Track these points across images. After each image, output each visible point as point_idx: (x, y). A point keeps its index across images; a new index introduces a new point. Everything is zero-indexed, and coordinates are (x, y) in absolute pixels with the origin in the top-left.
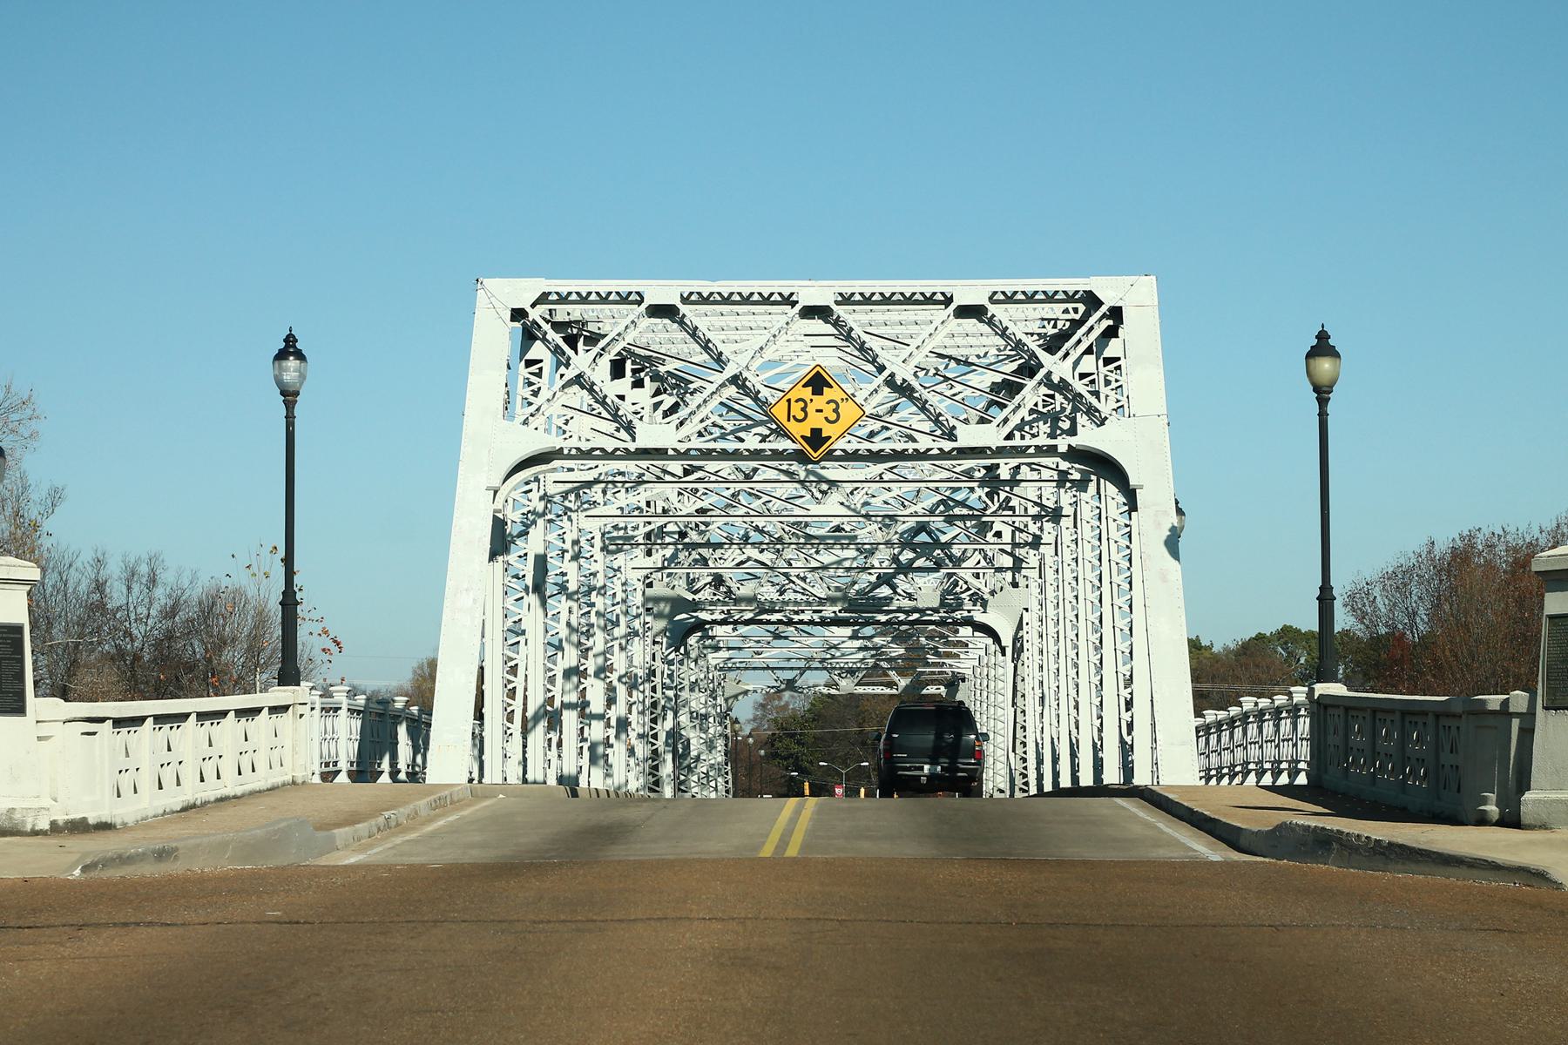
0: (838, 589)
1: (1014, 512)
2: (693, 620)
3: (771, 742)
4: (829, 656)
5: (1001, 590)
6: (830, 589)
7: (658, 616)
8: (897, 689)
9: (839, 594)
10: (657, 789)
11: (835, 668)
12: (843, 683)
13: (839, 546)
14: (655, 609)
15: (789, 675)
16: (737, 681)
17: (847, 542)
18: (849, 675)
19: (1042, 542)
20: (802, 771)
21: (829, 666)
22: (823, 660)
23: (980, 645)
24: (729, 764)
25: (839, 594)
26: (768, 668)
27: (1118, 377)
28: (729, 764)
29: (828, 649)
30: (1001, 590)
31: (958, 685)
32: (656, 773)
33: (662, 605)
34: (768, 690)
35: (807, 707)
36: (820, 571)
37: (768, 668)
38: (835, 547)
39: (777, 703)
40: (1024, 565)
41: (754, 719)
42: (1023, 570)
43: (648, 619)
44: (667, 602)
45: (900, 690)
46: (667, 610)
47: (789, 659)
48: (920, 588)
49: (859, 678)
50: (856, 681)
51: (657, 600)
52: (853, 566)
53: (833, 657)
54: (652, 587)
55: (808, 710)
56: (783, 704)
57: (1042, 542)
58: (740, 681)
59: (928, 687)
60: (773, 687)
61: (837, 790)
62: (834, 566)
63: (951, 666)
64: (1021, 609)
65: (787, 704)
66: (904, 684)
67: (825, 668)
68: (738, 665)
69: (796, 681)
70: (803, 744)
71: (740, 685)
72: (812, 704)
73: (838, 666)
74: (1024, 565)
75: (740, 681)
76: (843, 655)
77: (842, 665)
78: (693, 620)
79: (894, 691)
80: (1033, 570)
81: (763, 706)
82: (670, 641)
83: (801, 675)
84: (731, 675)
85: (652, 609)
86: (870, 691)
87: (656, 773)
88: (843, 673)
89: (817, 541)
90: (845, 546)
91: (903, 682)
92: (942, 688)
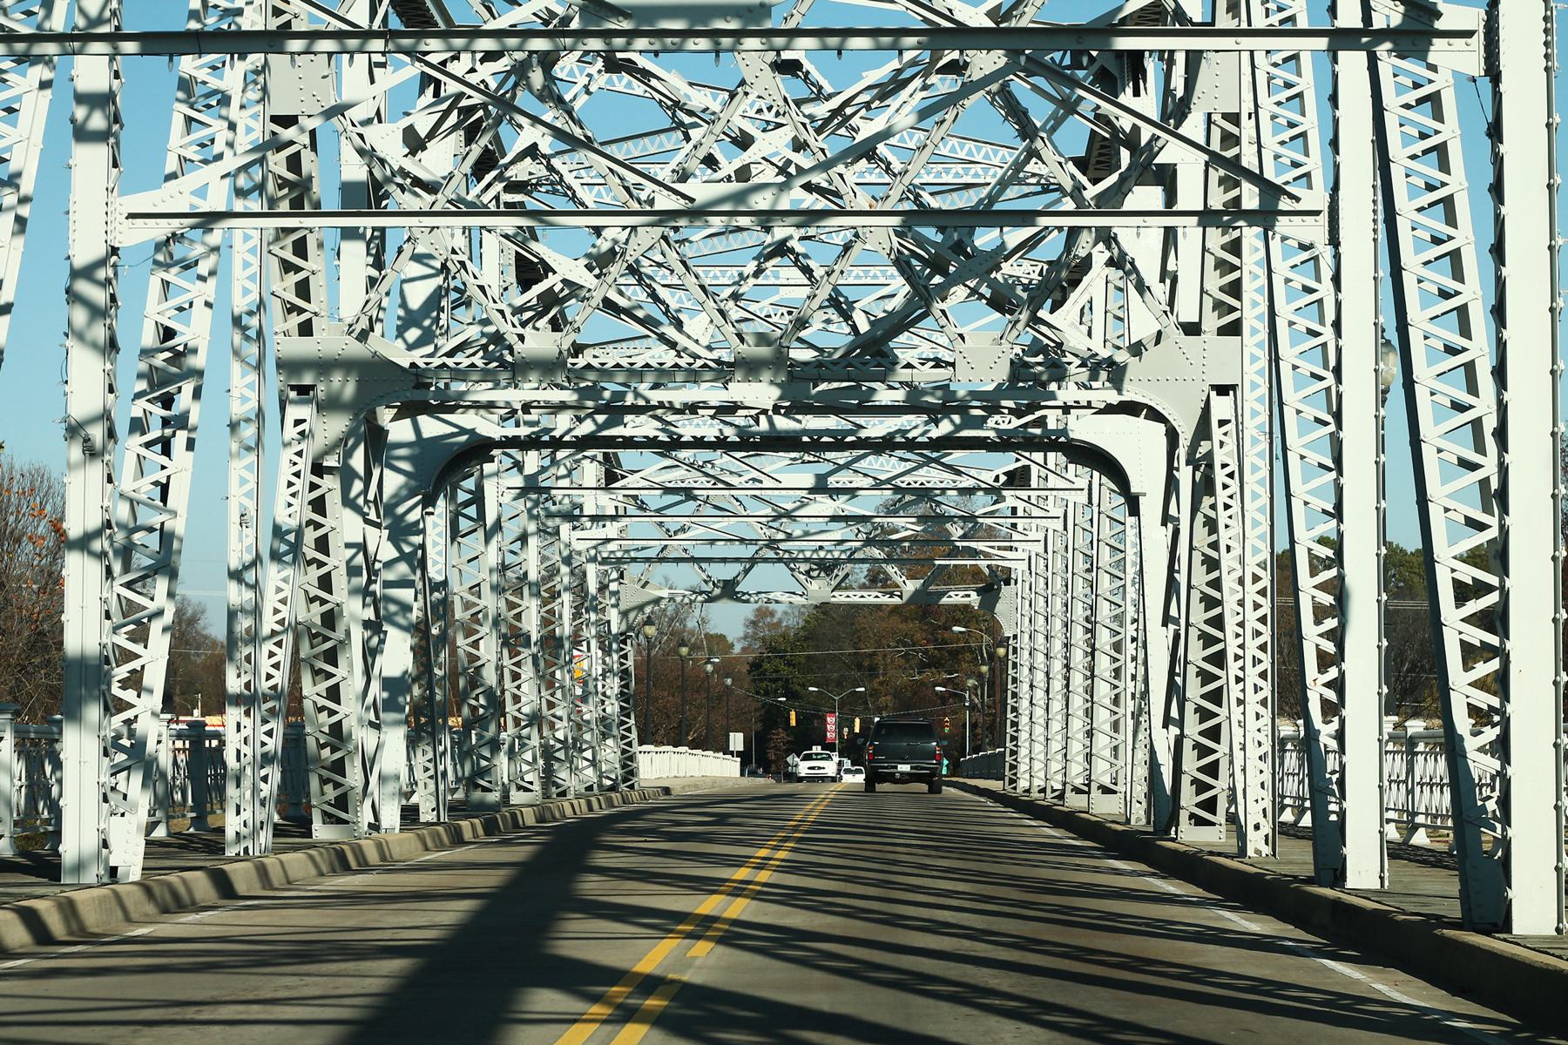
0: (762, 339)
1: (1171, 197)
2: (464, 438)
3: (756, 666)
4: (781, 536)
5: (1158, 342)
6: (742, 340)
7: (329, 406)
8: (901, 597)
9: (764, 351)
10: (343, 815)
11: (795, 560)
12: (814, 586)
13: (703, 43)
14: (321, 387)
15: (729, 571)
16: (642, 583)
17: (733, 25)
18: (822, 574)
19: (1440, 25)
20: (791, 695)
21: (787, 556)
22: (772, 543)
23: (1032, 535)
24: (633, 716)
25: (764, 351)
26: (693, 560)
27: (1292, 78)
28: (633, 716)
29: (776, 518)
30: (1158, 342)
31: (999, 589)
32: (339, 778)
33: (337, 378)
34: (693, 597)
35: (802, 624)
36: (682, 222)
37: (693, 560)
38: (691, 44)
39: (769, 619)
40: (1285, 204)
41: (745, 638)
42: (1282, 220)
43: (305, 412)
44: (347, 373)
45: (905, 598)
46: (349, 390)
47: (712, 541)
48: (961, 336)
49: (839, 579)
50: (834, 583)
51: (324, 366)
52: (781, 207)
53: (789, 537)
54: (310, 334)
55: (803, 628)
56: (775, 620)
57: (1440, 25)
58: (647, 583)
59: (951, 593)
60: (701, 593)
61: (829, 719)
62: (726, 207)
63: (987, 556)
64: (1207, 388)
65: (780, 621)
66: (913, 589)
67: (780, 560)
68: (633, 554)
69: (738, 583)
70: (794, 666)
71: (647, 589)
72: (807, 622)
73: (801, 556)
74: (1285, 204)
75: (647, 583)
76: (807, 533)
77: (808, 554)
78: (464, 438)
79: (896, 600)
80: (1459, 43)
81: (754, 623)
82: (413, 483)
83: (747, 571)
84: (633, 570)
85: (312, 387)
86: (857, 600)
87: (339, 778)
88: (811, 569)
89: (626, 25)
90: (726, 42)
91: (911, 586)
92: (974, 595)
